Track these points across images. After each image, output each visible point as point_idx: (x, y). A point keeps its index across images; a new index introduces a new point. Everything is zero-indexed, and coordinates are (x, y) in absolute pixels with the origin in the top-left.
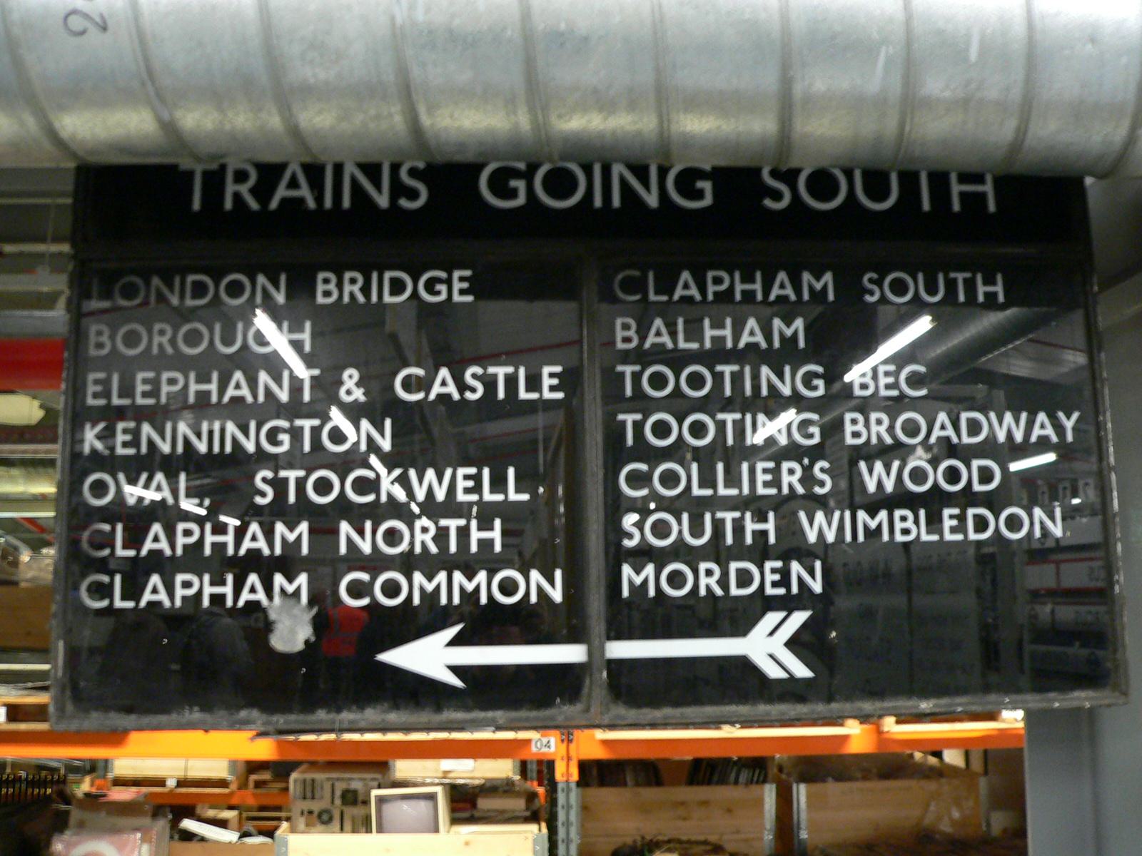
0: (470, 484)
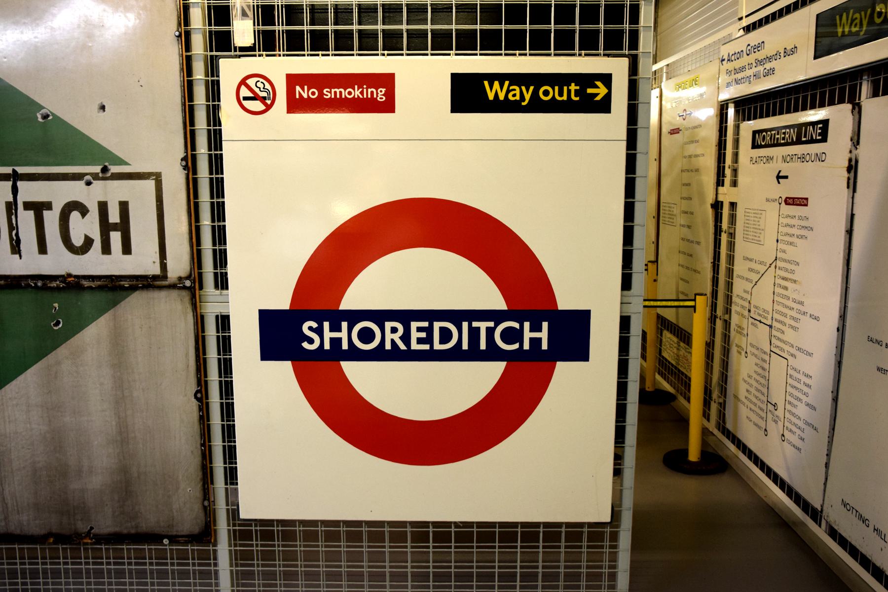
0: (423, 335)
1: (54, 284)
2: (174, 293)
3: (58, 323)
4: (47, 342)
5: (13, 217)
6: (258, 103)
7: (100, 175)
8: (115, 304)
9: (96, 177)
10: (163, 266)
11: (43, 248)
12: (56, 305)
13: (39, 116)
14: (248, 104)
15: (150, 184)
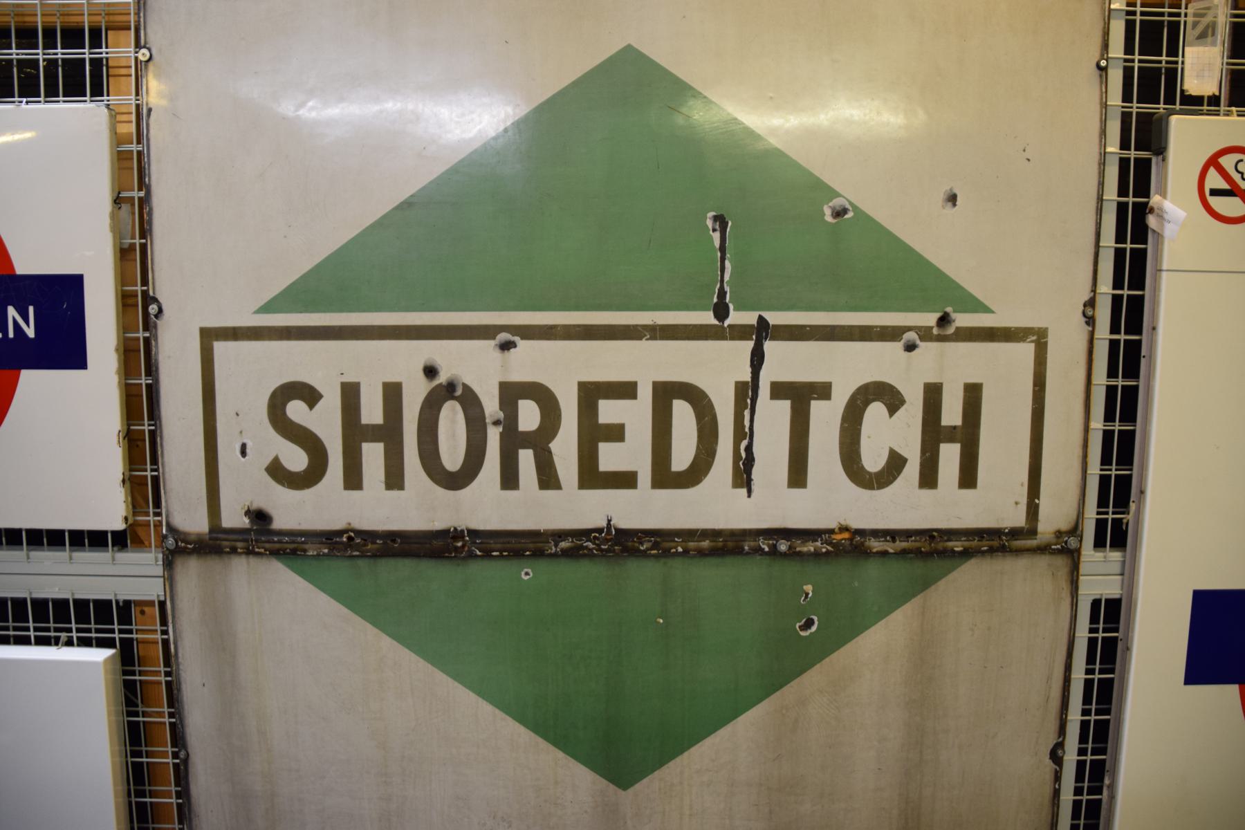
1: (810, 547)
2: (1043, 561)
3: (809, 623)
4: (788, 656)
5: (747, 413)
6: (1236, 201)
7: (935, 331)
8: (926, 584)
9: (925, 334)
10: (1033, 511)
11: (798, 475)
12: (809, 588)
13: (828, 212)
14: (1216, 203)
15: (1026, 350)
